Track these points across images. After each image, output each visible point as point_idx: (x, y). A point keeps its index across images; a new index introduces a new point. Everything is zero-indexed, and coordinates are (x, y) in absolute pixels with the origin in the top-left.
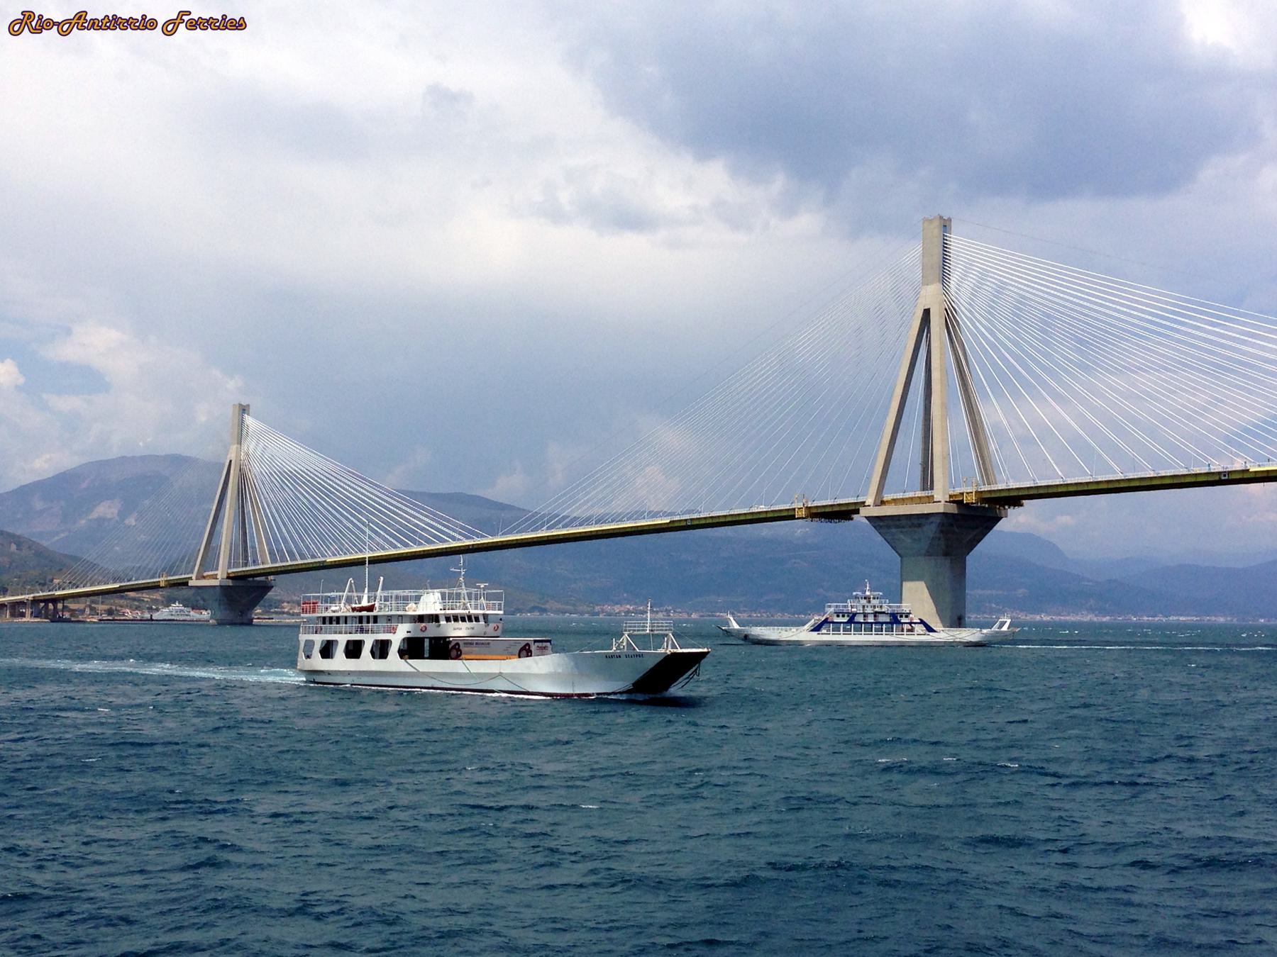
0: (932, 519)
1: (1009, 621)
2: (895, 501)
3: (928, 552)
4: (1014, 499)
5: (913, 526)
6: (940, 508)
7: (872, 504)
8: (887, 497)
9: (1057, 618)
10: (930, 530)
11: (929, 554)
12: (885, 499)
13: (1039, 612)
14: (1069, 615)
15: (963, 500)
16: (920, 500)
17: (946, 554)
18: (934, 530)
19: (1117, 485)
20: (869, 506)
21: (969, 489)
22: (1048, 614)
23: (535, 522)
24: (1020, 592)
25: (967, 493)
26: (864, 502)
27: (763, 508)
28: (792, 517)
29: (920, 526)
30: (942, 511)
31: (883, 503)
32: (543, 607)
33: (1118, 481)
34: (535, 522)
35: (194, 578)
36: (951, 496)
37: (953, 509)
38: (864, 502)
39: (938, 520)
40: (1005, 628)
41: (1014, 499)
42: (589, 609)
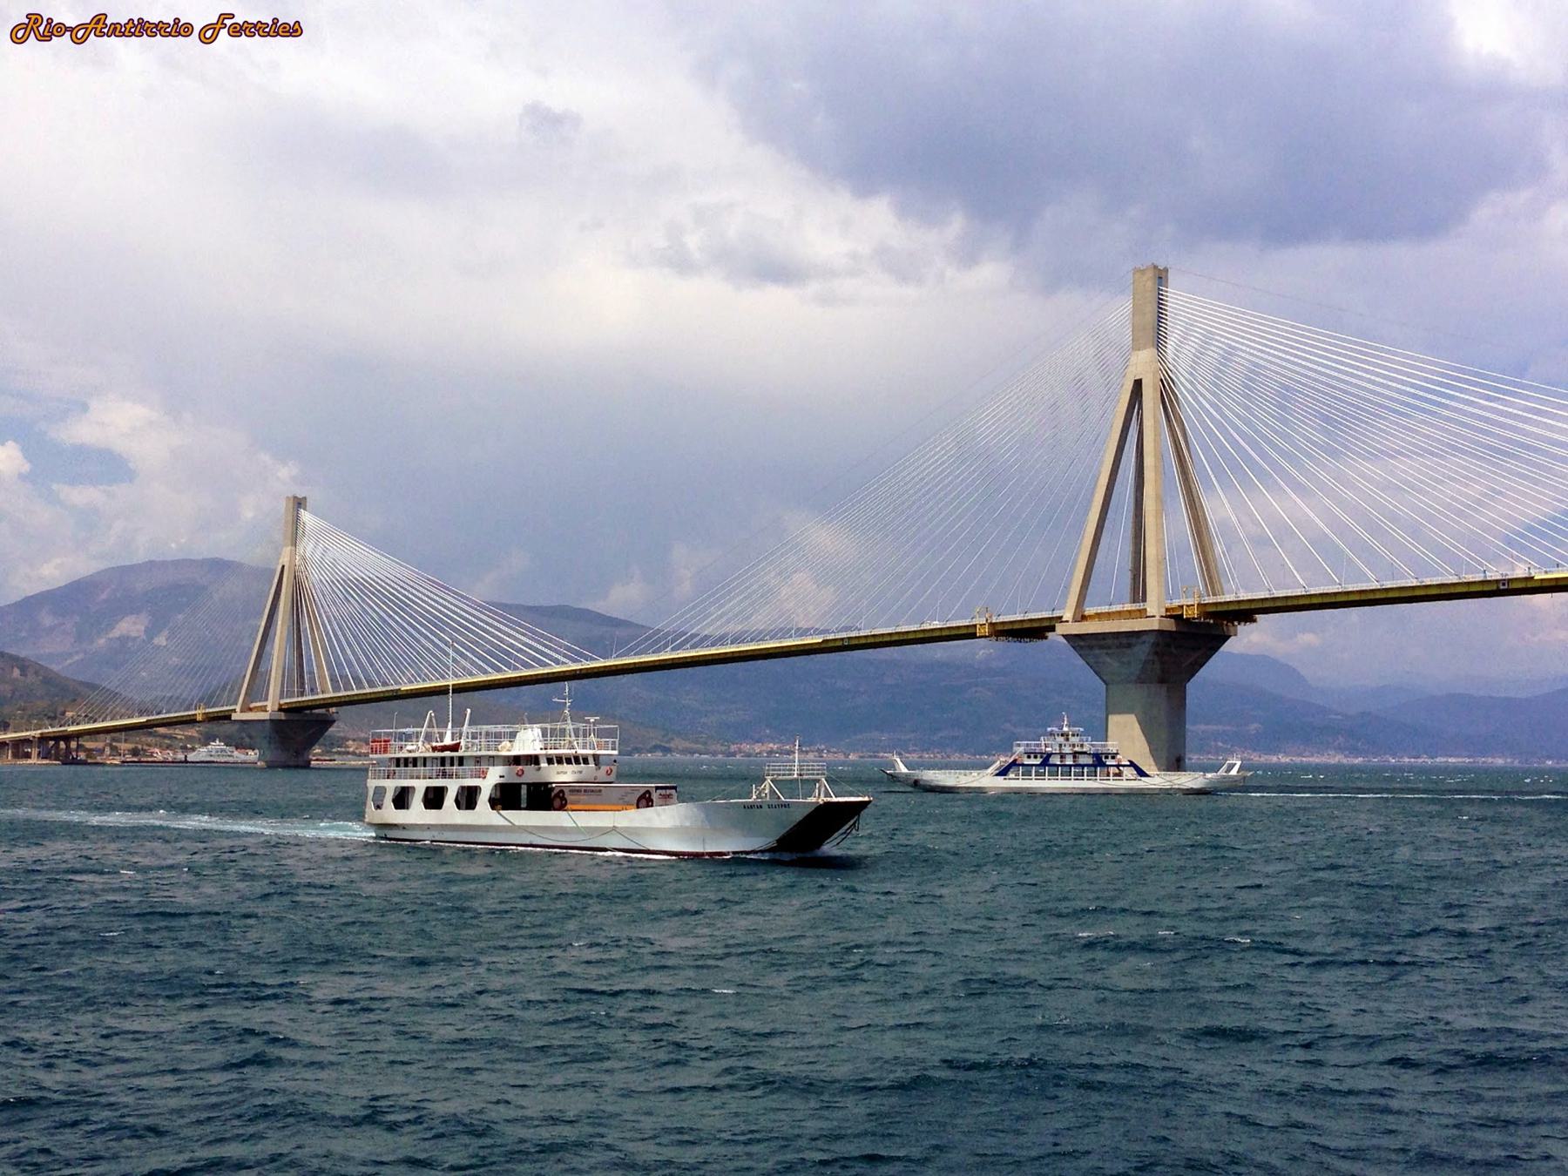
0: (1144, 638)
1: (1239, 763)
2: (1099, 616)
3: (1139, 678)
4: (1246, 613)
5: (1120, 646)
6: (1154, 625)
7: (1071, 620)
8: (1089, 611)
9: (1297, 760)
10: (1142, 651)
11: (1140, 680)
12: (1086, 613)
13: (1275, 751)
14: (1312, 756)
15: (1182, 615)
16: (1130, 614)
17: (1162, 681)
18: (1147, 650)
19: (1371, 596)
20: (1067, 621)
21: (1190, 600)
22: (1286, 754)
23: (656, 642)
24: (1253, 727)
25: (1188, 606)
26: (1061, 617)
27: (937, 624)
28: (973, 636)
29: (1129, 646)
30: (1156, 628)
31: (1084, 618)
32: (667, 745)
33: (1373, 591)
34: (656, 642)
35: (238, 710)
36: (1167, 610)
37: (1170, 625)
38: (1061, 617)
39: (1151, 639)
40: (1234, 772)
41: (1246, 613)
42: (724, 748)
